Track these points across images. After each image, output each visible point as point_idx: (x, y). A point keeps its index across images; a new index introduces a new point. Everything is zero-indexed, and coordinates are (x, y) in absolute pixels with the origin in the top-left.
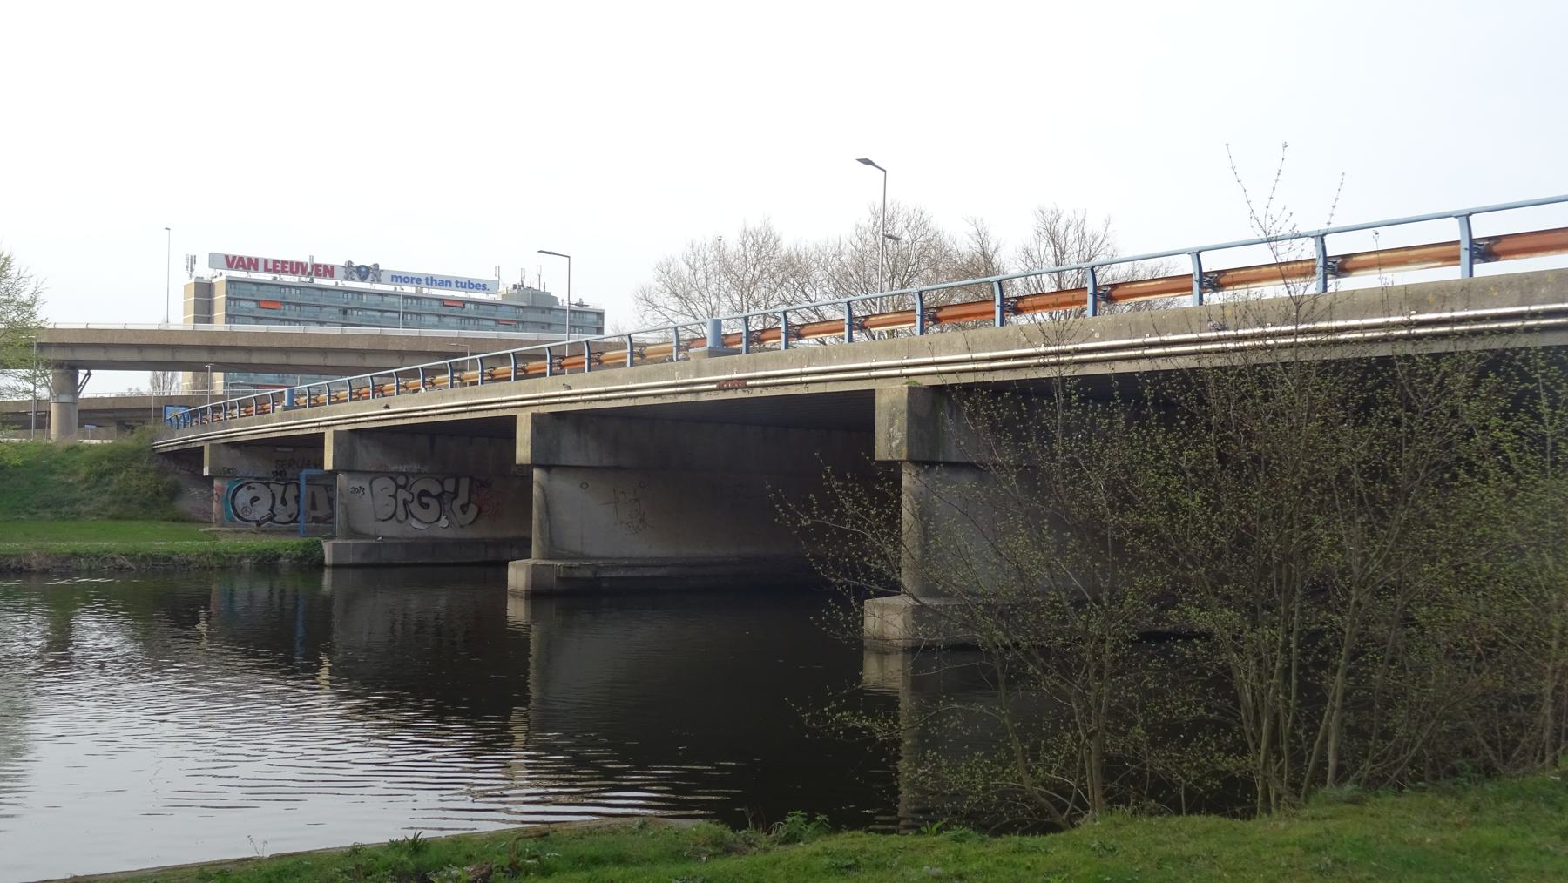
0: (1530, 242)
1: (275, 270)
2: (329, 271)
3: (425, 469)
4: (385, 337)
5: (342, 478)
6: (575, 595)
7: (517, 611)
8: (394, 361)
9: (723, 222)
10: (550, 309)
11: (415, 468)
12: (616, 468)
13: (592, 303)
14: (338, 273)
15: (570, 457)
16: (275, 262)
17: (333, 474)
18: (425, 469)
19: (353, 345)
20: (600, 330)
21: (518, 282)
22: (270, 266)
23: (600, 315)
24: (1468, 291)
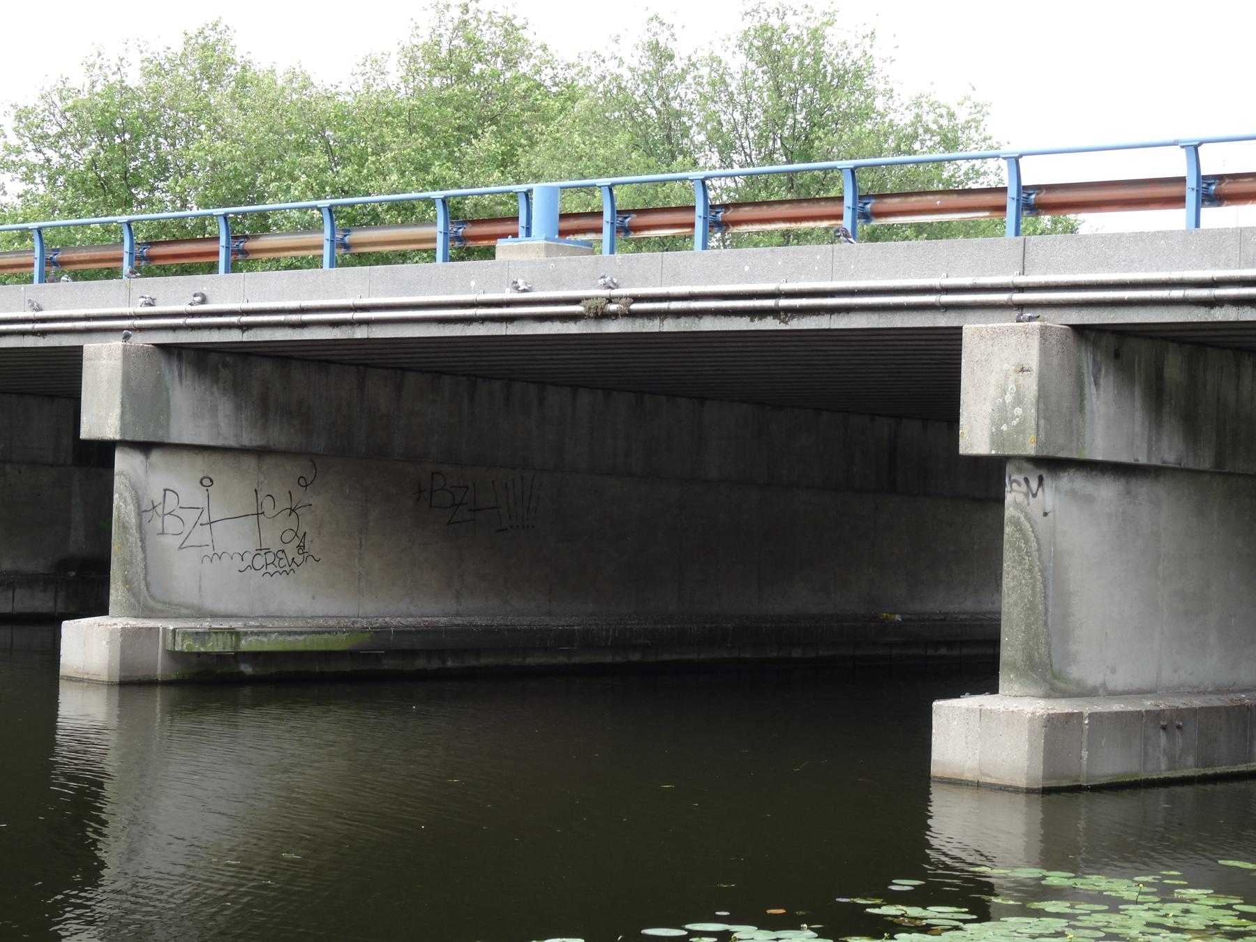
6: (210, 681)
7: (81, 710)
12: (260, 452)
15: (185, 429)
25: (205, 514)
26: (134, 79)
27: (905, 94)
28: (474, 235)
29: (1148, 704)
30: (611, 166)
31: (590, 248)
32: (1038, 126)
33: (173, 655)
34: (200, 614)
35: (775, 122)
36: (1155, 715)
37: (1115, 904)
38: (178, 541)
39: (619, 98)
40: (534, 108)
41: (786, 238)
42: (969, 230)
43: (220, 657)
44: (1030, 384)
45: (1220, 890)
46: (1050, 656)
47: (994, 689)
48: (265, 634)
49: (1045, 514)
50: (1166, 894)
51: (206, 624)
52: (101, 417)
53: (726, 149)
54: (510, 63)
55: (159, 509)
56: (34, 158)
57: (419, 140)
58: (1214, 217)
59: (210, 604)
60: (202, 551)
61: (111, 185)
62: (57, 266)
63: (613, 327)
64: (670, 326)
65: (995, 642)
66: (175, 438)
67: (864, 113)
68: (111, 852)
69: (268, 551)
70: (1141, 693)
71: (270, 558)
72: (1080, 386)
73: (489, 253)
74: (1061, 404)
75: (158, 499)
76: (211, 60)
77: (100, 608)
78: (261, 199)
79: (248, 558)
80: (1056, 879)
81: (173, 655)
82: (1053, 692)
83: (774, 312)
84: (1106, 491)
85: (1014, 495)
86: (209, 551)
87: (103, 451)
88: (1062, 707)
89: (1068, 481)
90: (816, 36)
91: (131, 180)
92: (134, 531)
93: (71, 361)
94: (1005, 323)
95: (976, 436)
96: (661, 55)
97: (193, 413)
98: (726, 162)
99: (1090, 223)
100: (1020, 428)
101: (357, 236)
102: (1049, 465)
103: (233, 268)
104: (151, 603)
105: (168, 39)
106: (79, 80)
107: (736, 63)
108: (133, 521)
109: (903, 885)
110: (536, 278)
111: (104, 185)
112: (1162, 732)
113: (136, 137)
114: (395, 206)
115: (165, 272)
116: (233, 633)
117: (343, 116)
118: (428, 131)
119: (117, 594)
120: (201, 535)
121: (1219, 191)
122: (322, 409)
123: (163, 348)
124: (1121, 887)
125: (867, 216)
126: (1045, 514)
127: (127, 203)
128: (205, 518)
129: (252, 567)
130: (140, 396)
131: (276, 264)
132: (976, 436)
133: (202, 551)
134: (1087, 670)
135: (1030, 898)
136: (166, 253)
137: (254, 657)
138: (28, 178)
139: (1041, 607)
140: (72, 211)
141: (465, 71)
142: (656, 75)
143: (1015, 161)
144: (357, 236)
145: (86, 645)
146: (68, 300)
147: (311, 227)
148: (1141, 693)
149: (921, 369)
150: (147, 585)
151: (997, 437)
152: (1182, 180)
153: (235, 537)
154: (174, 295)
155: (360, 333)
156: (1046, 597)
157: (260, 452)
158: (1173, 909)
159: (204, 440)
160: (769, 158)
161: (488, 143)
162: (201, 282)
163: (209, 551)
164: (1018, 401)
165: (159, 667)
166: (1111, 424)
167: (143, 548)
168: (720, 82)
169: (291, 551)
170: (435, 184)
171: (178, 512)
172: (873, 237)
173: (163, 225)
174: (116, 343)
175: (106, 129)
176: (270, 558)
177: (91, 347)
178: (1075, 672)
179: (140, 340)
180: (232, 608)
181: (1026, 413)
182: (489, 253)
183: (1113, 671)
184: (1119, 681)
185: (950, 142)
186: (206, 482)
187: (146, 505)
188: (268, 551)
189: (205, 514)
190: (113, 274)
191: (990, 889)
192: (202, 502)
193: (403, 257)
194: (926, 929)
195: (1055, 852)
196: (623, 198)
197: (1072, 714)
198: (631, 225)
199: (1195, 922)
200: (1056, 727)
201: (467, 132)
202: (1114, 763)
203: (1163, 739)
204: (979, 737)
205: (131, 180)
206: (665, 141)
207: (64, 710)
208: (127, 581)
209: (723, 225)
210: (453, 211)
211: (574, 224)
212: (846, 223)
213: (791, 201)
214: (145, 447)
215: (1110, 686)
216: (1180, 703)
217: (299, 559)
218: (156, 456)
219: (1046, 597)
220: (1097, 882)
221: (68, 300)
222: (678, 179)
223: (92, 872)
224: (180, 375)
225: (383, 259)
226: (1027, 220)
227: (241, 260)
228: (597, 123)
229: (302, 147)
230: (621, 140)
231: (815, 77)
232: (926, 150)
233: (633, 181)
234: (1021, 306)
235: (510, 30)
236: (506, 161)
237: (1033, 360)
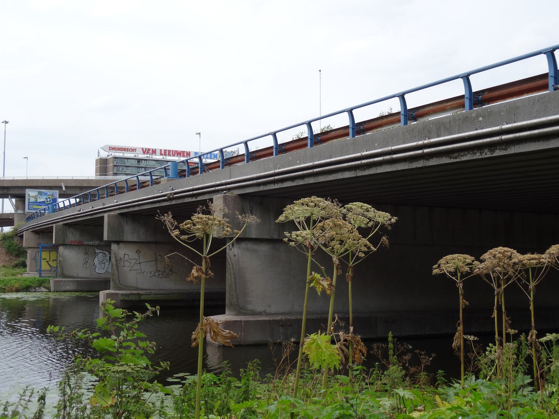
1: (165, 155)
14: (158, 152)
15: (129, 237)
22: (163, 152)
25: (138, 261)
36: (278, 322)
38: (129, 268)
46: (238, 302)
48: (149, 295)
49: (235, 256)
51: (129, 292)
55: (123, 260)
59: (140, 286)
66: (125, 239)
69: (159, 271)
70: (283, 314)
71: (160, 273)
75: (122, 256)
79: (153, 273)
82: (239, 313)
86: (140, 271)
92: (115, 266)
104: (120, 286)
108: (115, 263)
112: (281, 327)
120: (137, 267)
126: (235, 256)
128: (138, 262)
129: (154, 275)
139: (234, 286)
150: (119, 281)
153: (148, 268)
156: (235, 283)
157: (156, 243)
159: (135, 240)
163: (140, 271)
167: (118, 271)
169: (167, 271)
171: (129, 260)
176: (160, 273)
178: (250, 307)
180: (147, 287)
183: (270, 306)
186: (138, 252)
187: (118, 258)
188: (159, 271)
189: (138, 261)
192: (137, 257)
197: (237, 321)
203: (281, 329)
214: (118, 242)
215: (268, 312)
217: (170, 273)
218: (121, 245)
219: (235, 283)
224: (127, 222)
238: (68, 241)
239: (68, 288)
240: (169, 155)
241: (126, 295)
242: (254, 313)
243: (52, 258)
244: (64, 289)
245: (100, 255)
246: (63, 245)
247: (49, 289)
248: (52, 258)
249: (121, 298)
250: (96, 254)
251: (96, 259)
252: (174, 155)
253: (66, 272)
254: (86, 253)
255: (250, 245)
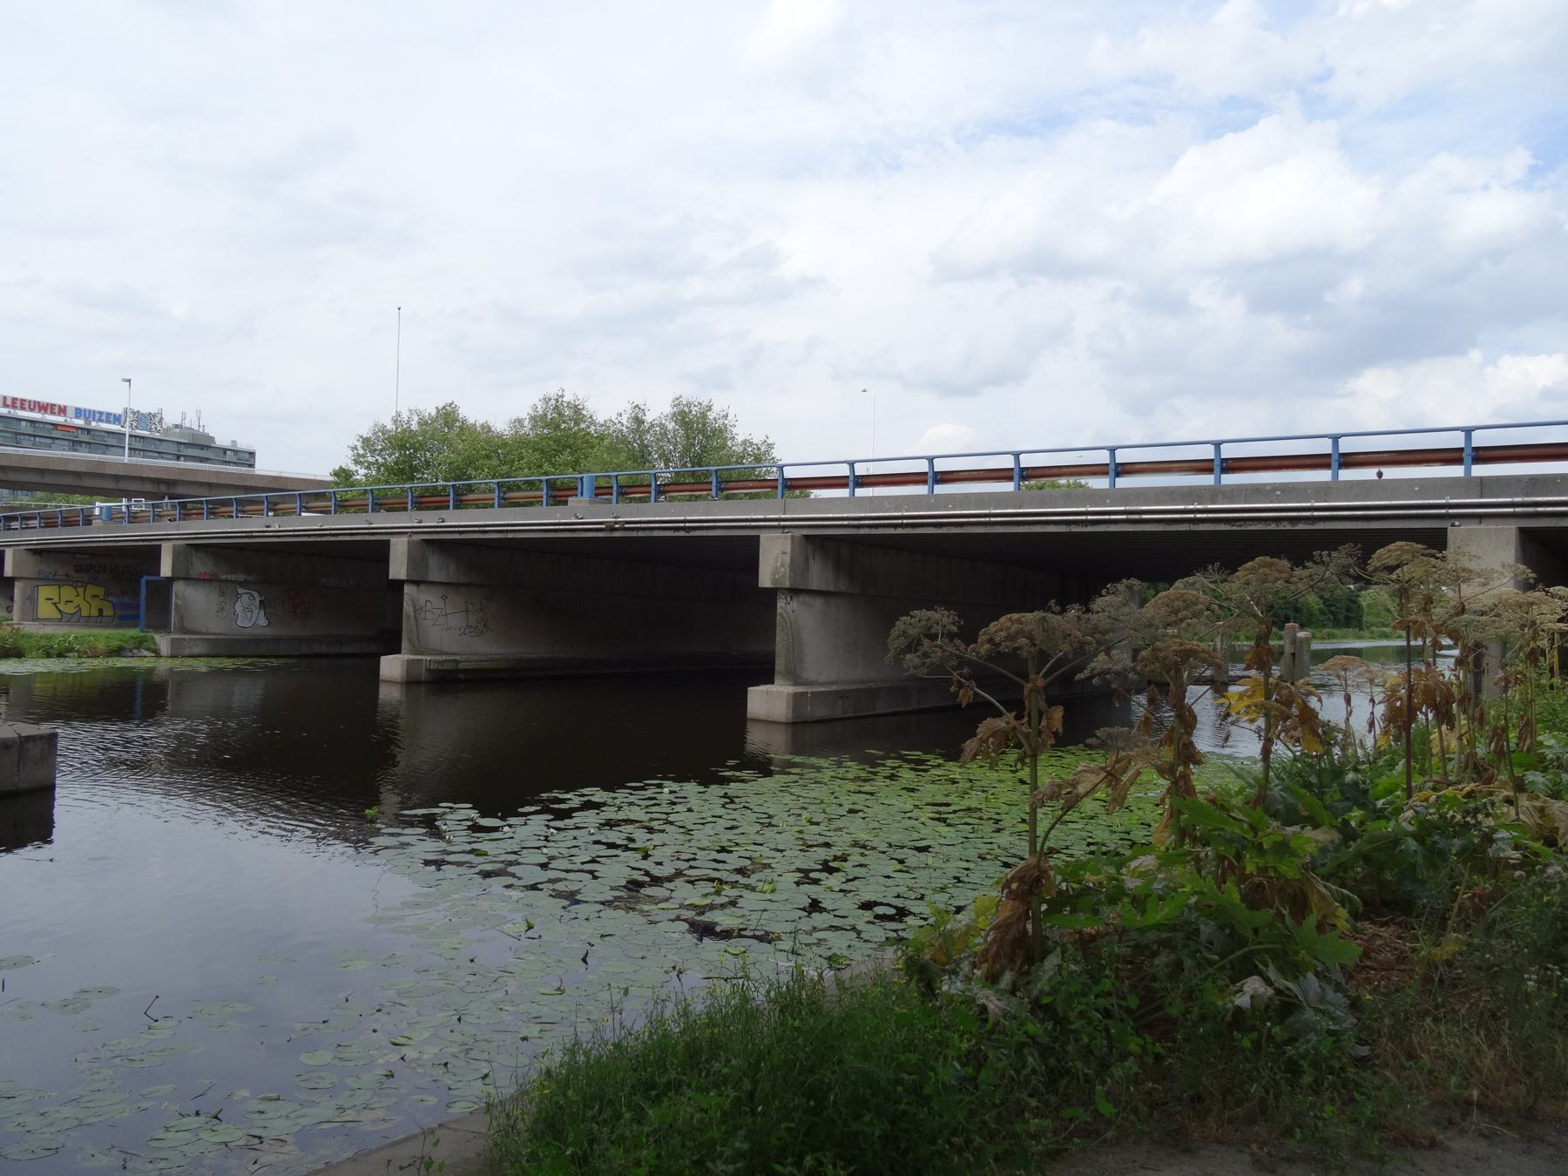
0: (1261, 463)
1: (14, 407)
2: (63, 410)
3: (251, 578)
4: (103, 463)
5: (178, 587)
6: (443, 681)
7: (389, 694)
8: (205, 491)
9: (409, 397)
10: (209, 447)
11: (241, 577)
12: (467, 585)
13: (243, 444)
14: (71, 413)
15: (435, 575)
16: (14, 400)
17: (170, 580)
18: (251, 578)
19: (71, 468)
20: (252, 466)
21: (178, 422)
22: (9, 402)
23: (252, 454)
24: (1216, 493)
26: (415, 427)
27: (740, 439)
28: (559, 494)
29: (834, 688)
30: (620, 467)
31: (609, 502)
32: (797, 452)
33: (429, 670)
34: (441, 653)
35: (687, 449)
36: (836, 692)
37: (819, 769)
39: (623, 439)
40: (587, 442)
41: (690, 499)
42: (766, 496)
43: (450, 671)
44: (787, 559)
45: (860, 763)
47: (772, 683)
50: (839, 765)
52: (398, 568)
53: (667, 461)
54: (577, 424)
56: (370, 459)
57: (537, 455)
58: (860, 492)
59: (446, 648)
60: (440, 627)
61: (405, 471)
62: (378, 506)
63: (617, 534)
64: (641, 534)
65: (773, 663)
67: (724, 446)
68: (401, 757)
70: (832, 683)
72: (807, 559)
73: (566, 503)
74: (799, 566)
76: (448, 416)
77: (399, 652)
78: (470, 478)
80: (797, 759)
81: (429, 670)
82: (796, 684)
83: (684, 529)
84: (818, 602)
85: (781, 604)
87: (399, 585)
88: (800, 689)
89: (802, 598)
90: (704, 415)
91: (414, 469)
93: (387, 544)
94: (777, 534)
95: (765, 580)
96: (639, 421)
97: (200, 566)
98: (667, 466)
99: (817, 493)
100: (783, 577)
101: (509, 495)
102: (794, 592)
103: (456, 507)
105: (430, 409)
106: (390, 426)
107: (671, 426)
109: (731, 763)
110: (584, 514)
111: (402, 471)
113: (416, 451)
114: (526, 482)
115: (428, 509)
116: (457, 662)
117: (505, 444)
118: (542, 451)
119: (405, 645)
121: (1349, 461)
122: (486, 566)
123: (807, 537)
124: (823, 762)
125: (722, 490)
127: (412, 479)
130: (414, 561)
131: (478, 507)
132: (765, 580)
133: (440, 627)
134: (810, 674)
135: (786, 767)
136: (425, 501)
137: (464, 671)
138: (368, 468)
140: (387, 482)
141: (558, 426)
142: (637, 430)
143: (781, 468)
144: (509, 495)
145: (391, 666)
146: (383, 521)
147: (492, 491)
148: (832, 683)
149: (377, 551)
151: (774, 580)
152: (1461, 450)
153: (456, 621)
154: (430, 519)
155: (510, 536)
157: (467, 585)
158: (842, 770)
160: (685, 465)
161: (566, 456)
162: (443, 513)
164: (782, 565)
165: (424, 676)
166: (819, 576)
168: (664, 433)
170: (546, 474)
172: (727, 498)
173: (427, 489)
174: (405, 539)
175: (402, 447)
177: (393, 540)
178: (805, 675)
179: (416, 538)
181: (785, 570)
182: (566, 503)
184: (822, 679)
185: (758, 459)
186: (444, 598)
190: (405, 509)
191: (770, 761)
193: (531, 504)
194: (743, 781)
195: (798, 747)
196: (622, 481)
198: (625, 492)
199: (850, 776)
200: (797, 698)
201: (558, 452)
202: (821, 712)
204: (767, 701)
205: (414, 469)
206: (641, 457)
207: (750, 737)
208: (410, 640)
209: (663, 493)
210: (551, 485)
211: (601, 491)
212: (713, 493)
213: (691, 484)
214: (417, 583)
216: (848, 687)
220: (814, 760)
221: (383, 521)
222: (645, 473)
223: (391, 761)
225: (524, 505)
226: (787, 493)
227: (460, 504)
228: (613, 449)
229: (488, 457)
230: (623, 456)
231: (703, 431)
232: (748, 462)
233: (624, 476)
234: (1481, 517)
235: (577, 410)
236: (575, 465)
237: (788, 549)
238: (194, 573)
239: (196, 650)
240: (23, 408)
241: (440, 662)
242: (811, 684)
243: (64, 598)
244: (187, 652)
245: (245, 597)
246: (184, 579)
247: (158, 654)
248: (64, 598)
249: (1366, 633)
250: (237, 596)
251: (238, 605)
252: (32, 410)
253: (186, 624)
254: (223, 594)
255: (807, 599)
